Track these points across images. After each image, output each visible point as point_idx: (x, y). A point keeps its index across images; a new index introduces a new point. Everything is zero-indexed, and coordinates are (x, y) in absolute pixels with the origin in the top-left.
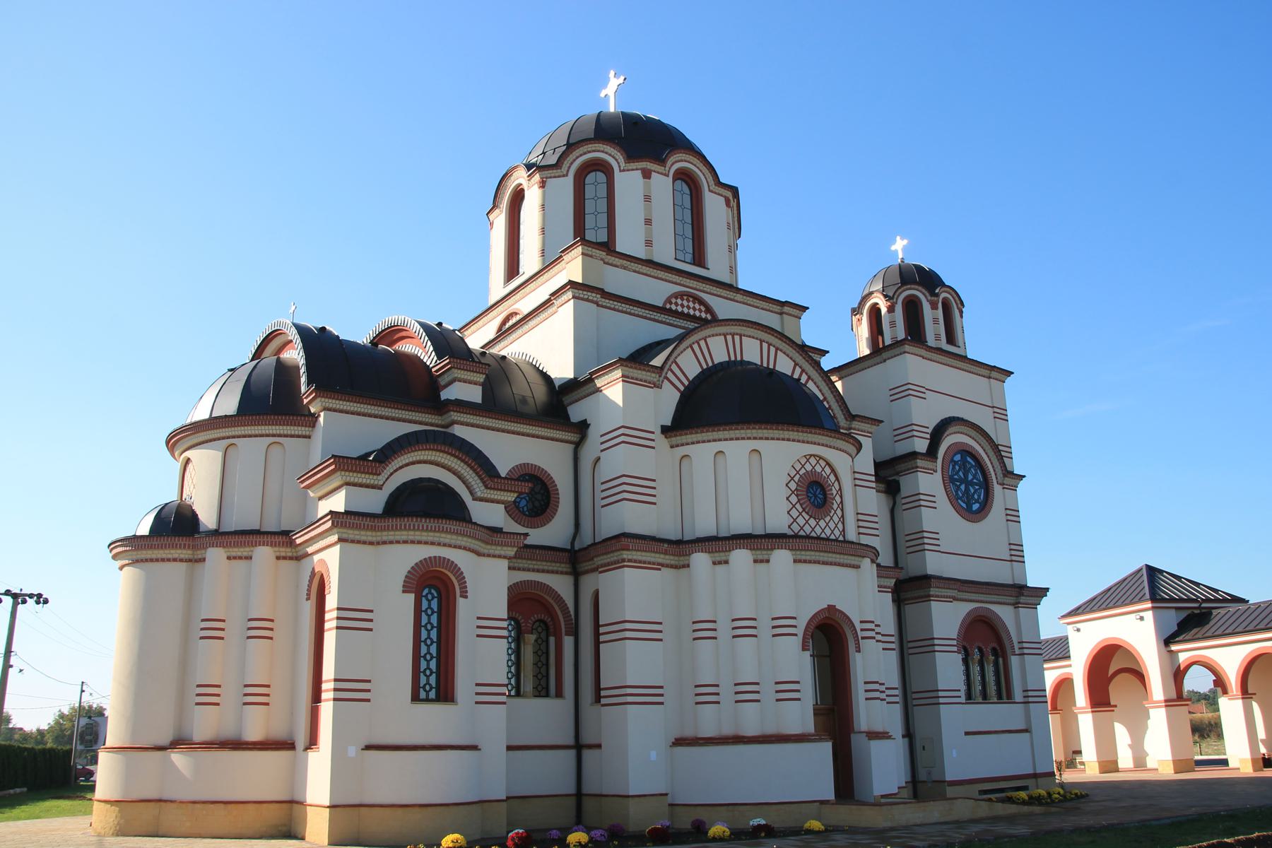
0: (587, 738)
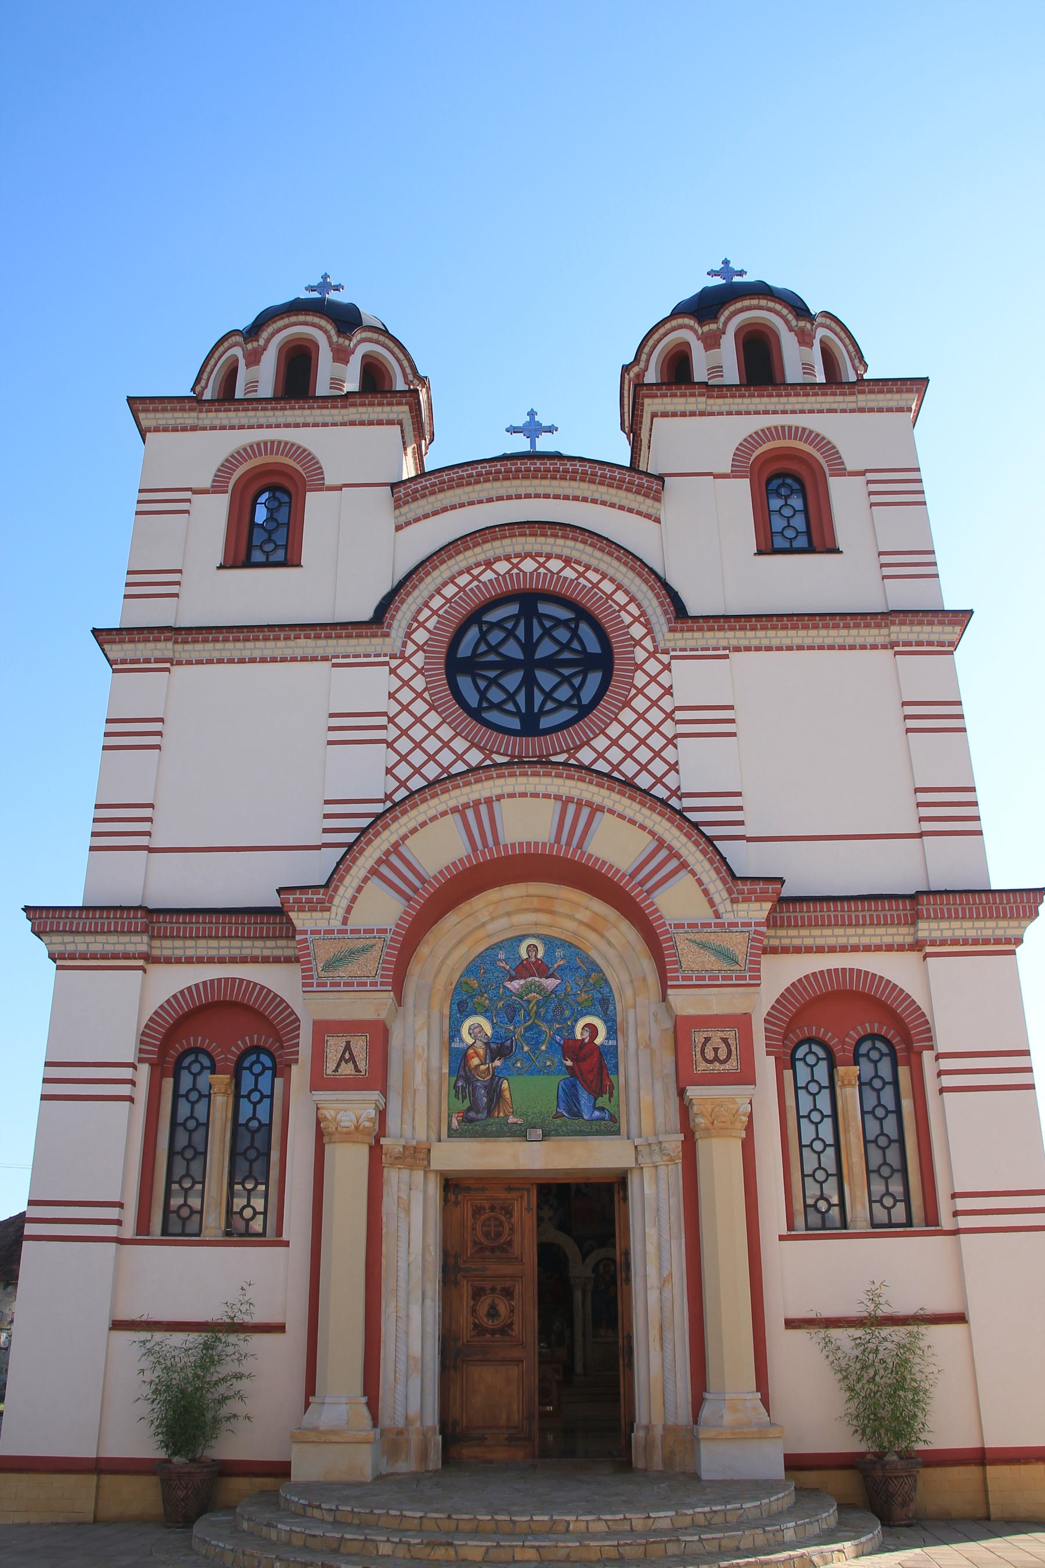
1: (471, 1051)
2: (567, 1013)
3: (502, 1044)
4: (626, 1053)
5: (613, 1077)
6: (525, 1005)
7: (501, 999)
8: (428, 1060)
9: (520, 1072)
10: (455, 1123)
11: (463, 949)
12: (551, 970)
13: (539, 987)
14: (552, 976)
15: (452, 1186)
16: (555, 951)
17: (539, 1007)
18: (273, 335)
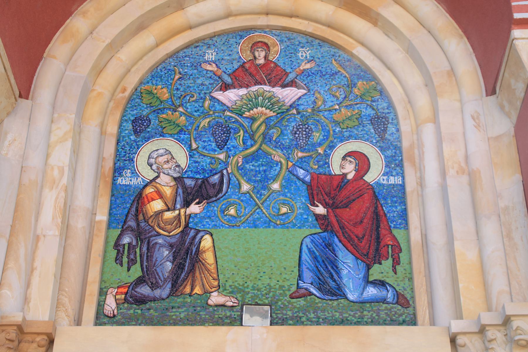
1: (149, 190)
2: (317, 136)
3: (205, 181)
4: (422, 197)
5: (399, 234)
6: (246, 124)
7: (206, 115)
8: (69, 192)
9: (233, 223)
10: (111, 305)
11: (146, 39)
12: (291, 76)
13: (270, 98)
14: (292, 84)
16: (297, 51)
17: (268, 128)
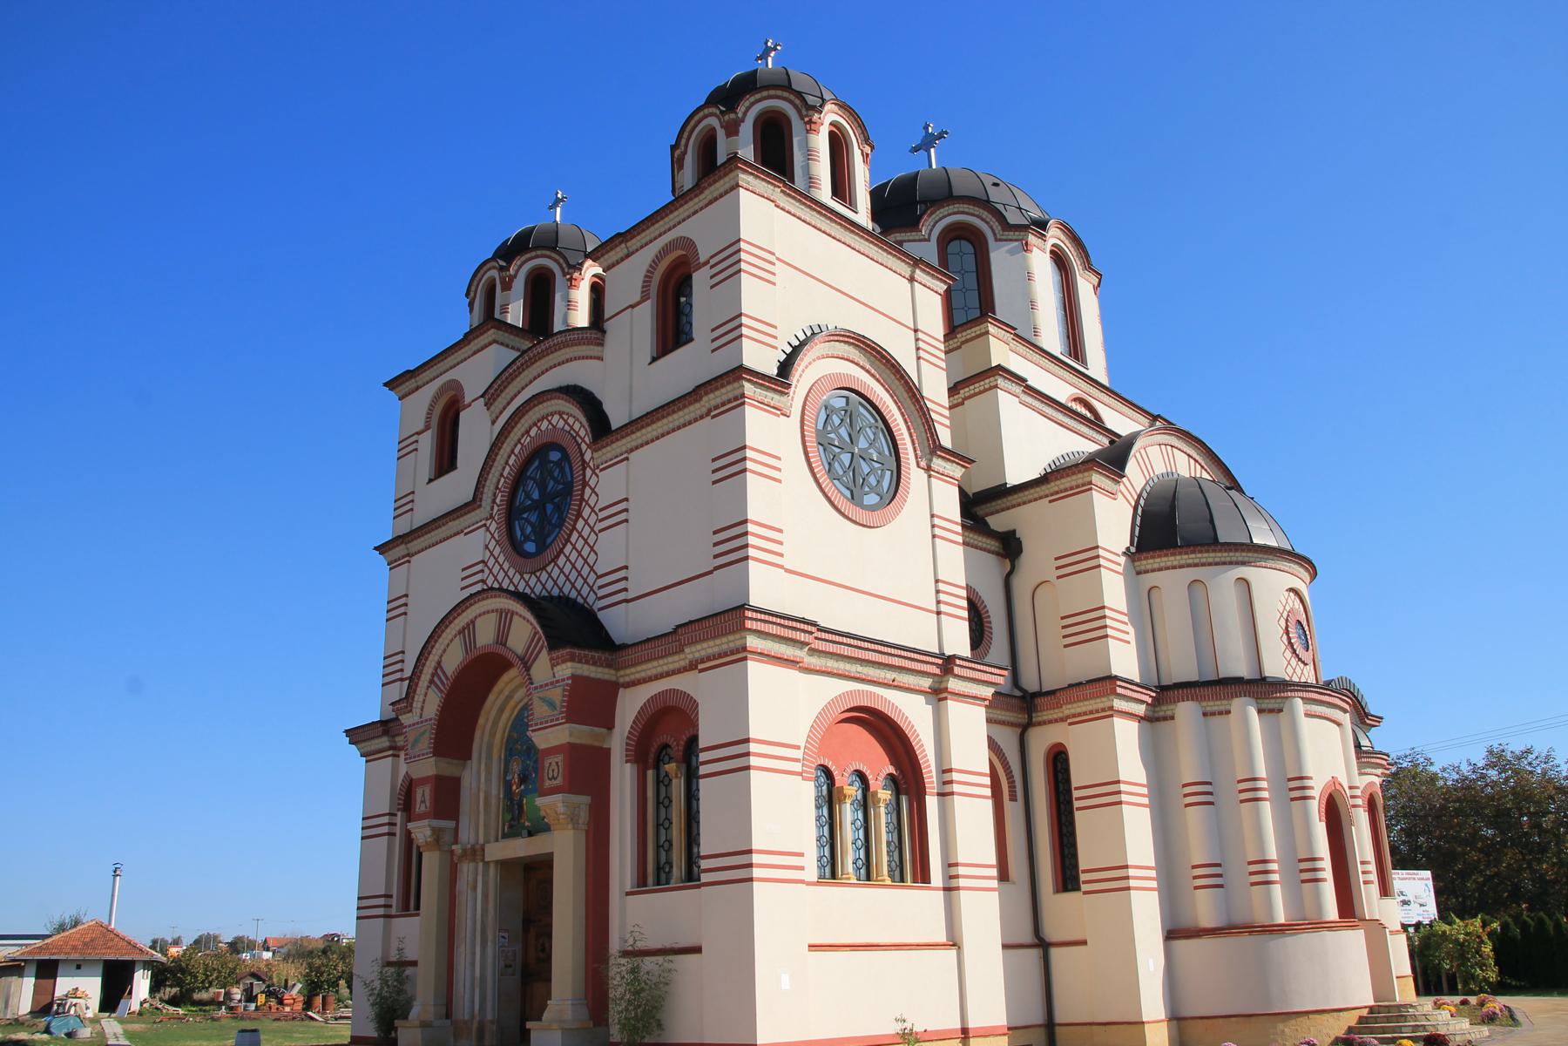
0: (1052, 932)
15: (505, 865)
18: (753, 104)
